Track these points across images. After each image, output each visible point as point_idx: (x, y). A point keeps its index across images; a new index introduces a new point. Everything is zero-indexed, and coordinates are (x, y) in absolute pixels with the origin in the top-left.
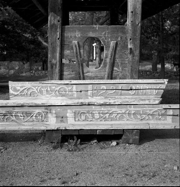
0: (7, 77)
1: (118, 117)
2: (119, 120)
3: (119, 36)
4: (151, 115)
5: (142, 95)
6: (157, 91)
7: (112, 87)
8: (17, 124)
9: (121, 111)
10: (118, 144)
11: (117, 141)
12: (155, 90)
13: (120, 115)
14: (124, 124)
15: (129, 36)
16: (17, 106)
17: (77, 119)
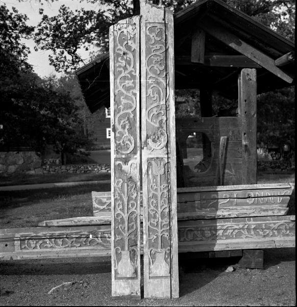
0: (4, 177)
1: (234, 233)
2: (236, 238)
3: (230, 130)
4: (276, 230)
5: (263, 204)
6: (281, 198)
7: (225, 195)
8: (103, 248)
9: (238, 225)
10: (235, 270)
11: (234, 266)
12: (278, 198)
13: (236, 231)
14: (242, 243)
15: (243, 127)
16: (103, 225)
17: (23, 247)
